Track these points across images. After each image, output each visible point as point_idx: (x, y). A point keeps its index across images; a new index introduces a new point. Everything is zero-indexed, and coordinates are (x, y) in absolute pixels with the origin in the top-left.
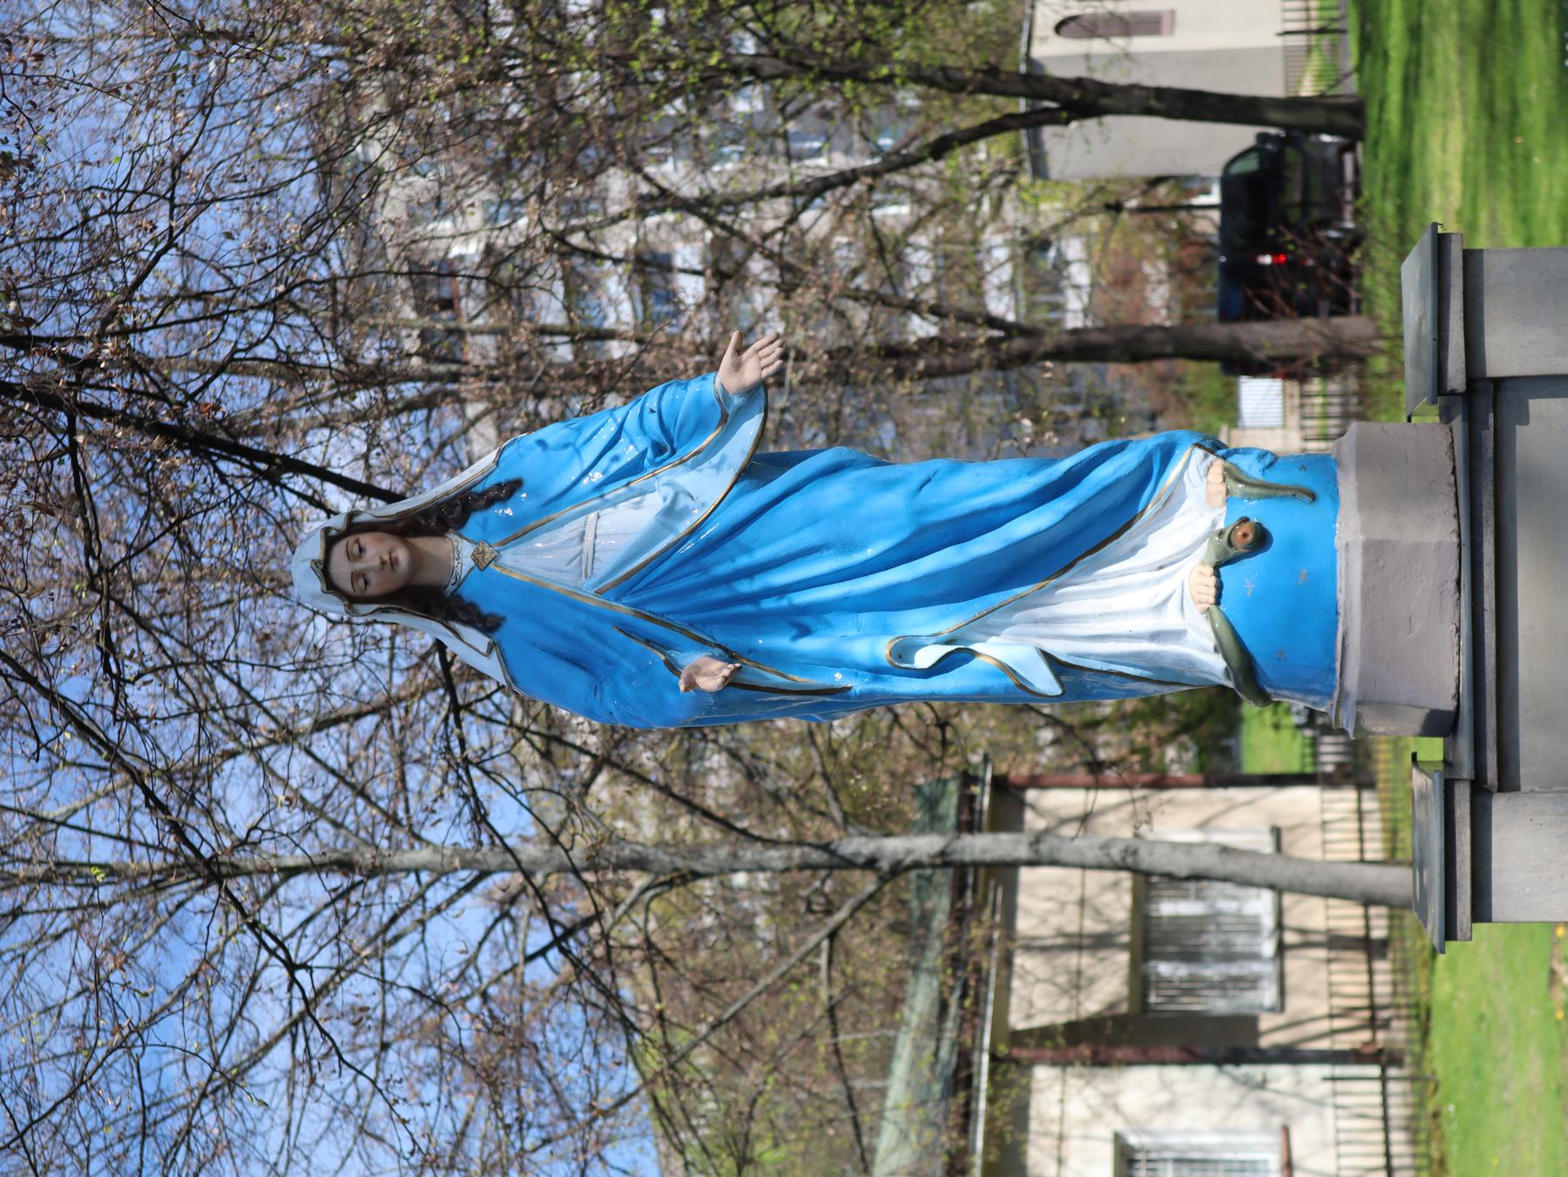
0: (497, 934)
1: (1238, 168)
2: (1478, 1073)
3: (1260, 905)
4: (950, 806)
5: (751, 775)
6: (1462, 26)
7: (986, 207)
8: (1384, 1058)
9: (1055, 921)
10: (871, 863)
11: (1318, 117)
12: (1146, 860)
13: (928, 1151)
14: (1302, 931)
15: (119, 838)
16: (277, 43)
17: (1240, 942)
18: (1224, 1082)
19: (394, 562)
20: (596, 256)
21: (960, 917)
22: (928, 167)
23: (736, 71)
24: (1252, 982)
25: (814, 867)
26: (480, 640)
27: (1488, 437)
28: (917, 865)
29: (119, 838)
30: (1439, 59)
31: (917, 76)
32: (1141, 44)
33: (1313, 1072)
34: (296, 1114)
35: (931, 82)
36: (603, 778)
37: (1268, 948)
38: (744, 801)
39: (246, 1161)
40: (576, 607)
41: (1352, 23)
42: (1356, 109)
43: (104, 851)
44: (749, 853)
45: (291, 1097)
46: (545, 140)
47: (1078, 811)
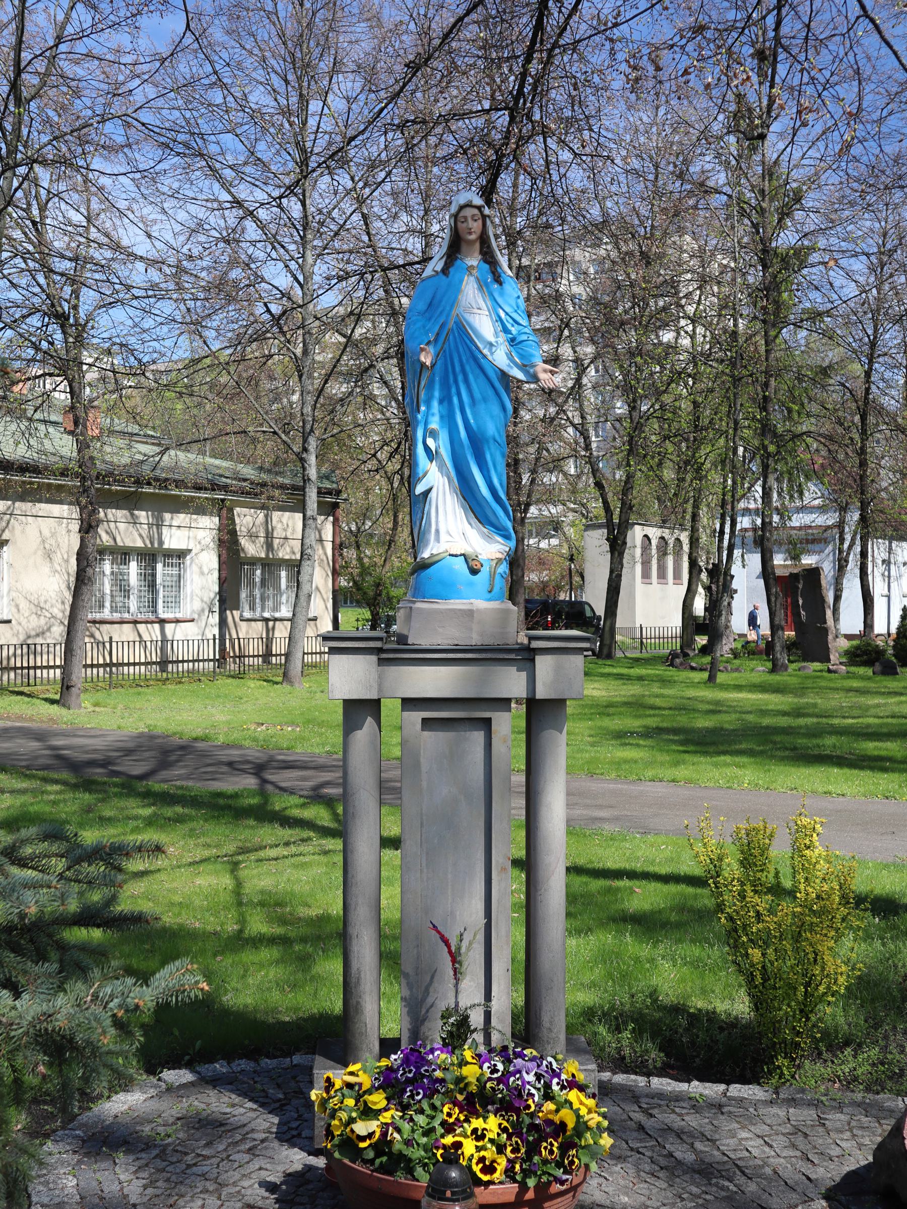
0: (275, 292)
1: (587, 607)
2: (219, 696)
3: (285, 611)
4: (327, 485)
5: (342, 400)
6: (644, 696)
7: (572, 506)
8: (222, 659)
9: (279, 526)
10: (305, 450)
11: (607, 642)
12: (306, 565)
13: (186, 471)
14: (273, 628)
15: (318, 128)
16: (653, 205)
17: (270, 603)
18: (212, 595)
19: (470, 233)
20: (559, 340)
21: (282, 487)
22: (591, 480)
23: (634, 401)
24: (252, 608)
25: (303, 427)
26: (439, 268)
27: (513, 656)
28: (304, 469)
29: (318, 128)
30: (630, 687)
31: (629, 477)
32: (638, 568)
33: (216, 631)
34: (199, 202)
35: (626, 482)
36: (342, 340)
37: (266, 615)
38: (330, 398)
39: (180, 180)
40: (452, 306)
41: (645, 655)
42: (609, 656)
43: (312, 122)
44: (310, 399)
45: (207, 201)
46: (609, 319)
47: (324, 538)
